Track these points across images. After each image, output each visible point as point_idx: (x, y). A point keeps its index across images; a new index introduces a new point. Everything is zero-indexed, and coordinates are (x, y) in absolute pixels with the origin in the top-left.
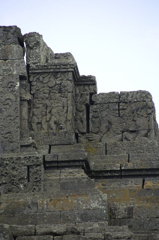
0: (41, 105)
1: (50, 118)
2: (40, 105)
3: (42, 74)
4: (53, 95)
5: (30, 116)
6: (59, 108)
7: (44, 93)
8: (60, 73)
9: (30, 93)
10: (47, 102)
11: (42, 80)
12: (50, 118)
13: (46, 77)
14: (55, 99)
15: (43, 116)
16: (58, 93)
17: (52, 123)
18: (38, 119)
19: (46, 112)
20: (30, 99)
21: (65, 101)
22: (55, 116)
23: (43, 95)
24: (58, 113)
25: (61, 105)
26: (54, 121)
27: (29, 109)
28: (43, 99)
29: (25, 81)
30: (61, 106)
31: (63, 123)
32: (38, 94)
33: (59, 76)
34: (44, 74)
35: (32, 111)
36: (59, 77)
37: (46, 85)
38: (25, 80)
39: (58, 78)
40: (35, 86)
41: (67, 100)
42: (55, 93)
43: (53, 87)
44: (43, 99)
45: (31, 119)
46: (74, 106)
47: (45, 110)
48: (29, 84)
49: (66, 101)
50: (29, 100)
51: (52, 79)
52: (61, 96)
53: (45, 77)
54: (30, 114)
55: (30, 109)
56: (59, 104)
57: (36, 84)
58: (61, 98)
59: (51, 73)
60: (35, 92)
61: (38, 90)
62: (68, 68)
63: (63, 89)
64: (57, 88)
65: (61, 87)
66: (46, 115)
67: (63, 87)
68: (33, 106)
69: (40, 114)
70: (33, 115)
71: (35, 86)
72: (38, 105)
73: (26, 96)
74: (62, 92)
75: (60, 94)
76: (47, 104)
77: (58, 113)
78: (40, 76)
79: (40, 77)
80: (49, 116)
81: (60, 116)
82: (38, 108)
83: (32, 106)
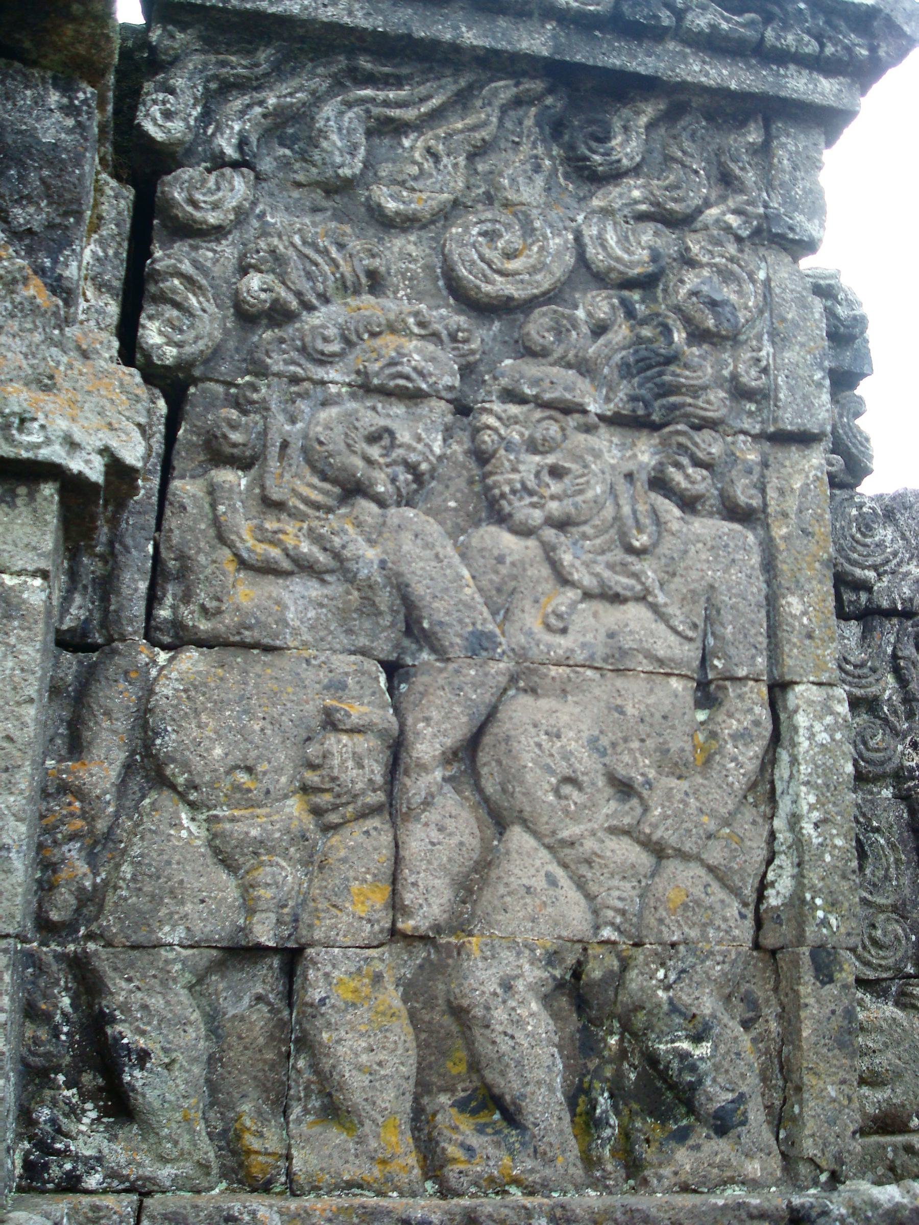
0: (314, 590)
1: (474, 881)
2: (297, 603)
3: (365, 63)
4: (533, 447)
5: (79, 793)
6: (637, 695)
7: (365, 388)
8: (649, 111)
9: (130, 350)
10: (424, 550)
11: (352, 168)
12: (474, 881)
13: (417, 126)
14: (562, 524)
15: (328, 808)
16: (615, 421)
17: (507, 986)
18: (224, 856)
19: (397, 750)
20: (133, 453)
21: (741, 580)
22: (557, 848)
23: (350, 420)
24: (624, 788)
25: (666, 644)
26: (552, 958)
27: (68, 641)
28: (352, 489)
29: (54, 98)
30: (664, 669)
31: (707, 1004)
32: (269, 392)
33: (626, 147)
34: (398, 82)
35: (116, 698)
36: (636, 171)
37: (404, 252)
38: (67, 87)
39: (615, 175)
40: (228, 250)
41: (769, 566)
42: (567, 409)
43: (529, 305)
44: (352, 489)
45: (101, 845)
46: (397, 612)
47: (367, 706)
48: (116, 202)
49: (758, 588)
50: (94, 470)
51: (525, 172)
52: (659, 483)
53: (399, 128)
54: (77, 746)
55: (82, 644)
56: (635, 613)
57: (241, 215)
58: (671, 510)
59: (505, 89)
60: (216, 352)
61: (279, 315)
62: (782, 58)
63: (702, 367)
64: (600, 329)
65: (667, 331)
66: (392, 808)
67: (698, 335)
68: (153, 599)
69: (280, 765)
70: (149, 768)
71: (218, 232)
72: (247, 594)
73: (45, 383)
74: (673, 413)
75: (645, 453)
76: (419, 589)
77: (624, 788)
78: (318, 99)
79: (328, 110)
80: (443, 832)
81: (658, 851)
82: (268, 649)
83: (135, 585)
